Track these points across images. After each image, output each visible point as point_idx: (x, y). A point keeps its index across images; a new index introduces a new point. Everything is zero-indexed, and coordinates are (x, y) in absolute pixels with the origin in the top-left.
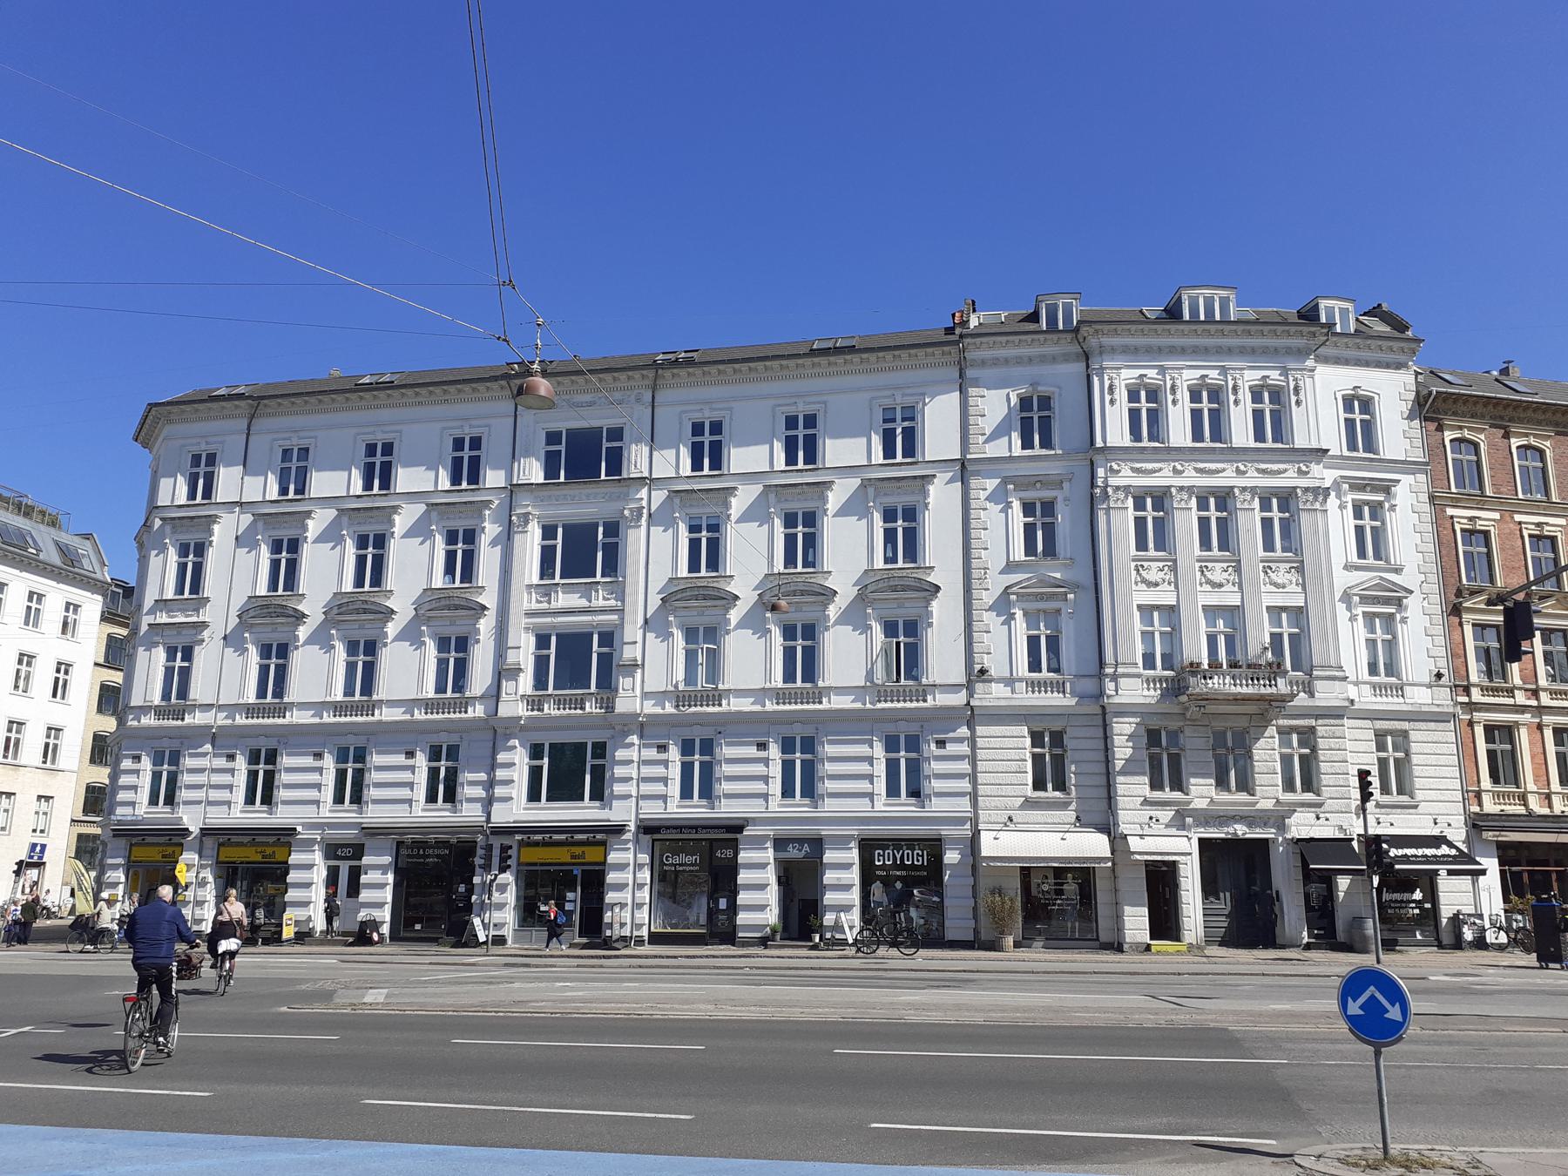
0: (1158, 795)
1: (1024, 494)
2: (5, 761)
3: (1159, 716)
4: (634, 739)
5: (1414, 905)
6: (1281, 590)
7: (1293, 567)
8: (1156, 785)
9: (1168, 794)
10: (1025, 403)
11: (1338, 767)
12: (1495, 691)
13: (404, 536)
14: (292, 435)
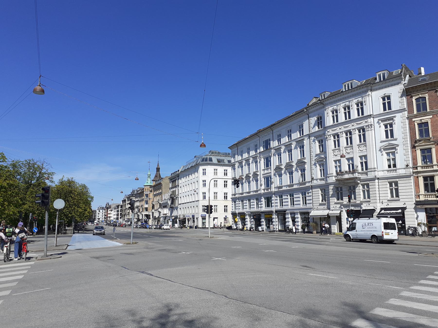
0: (338, 201)
1: (318, 139)
2: (215, 200)
3: (337, 184)
4: (274, 196)
5: (399, 225)
6: (362, 152)
7: (364, 146)
8: (338, 200)
9: (340, 201)
10: (318, 118)
11: (374, 192)
12: (427, 167)
13: (294, 149)
14: (278, 132)
